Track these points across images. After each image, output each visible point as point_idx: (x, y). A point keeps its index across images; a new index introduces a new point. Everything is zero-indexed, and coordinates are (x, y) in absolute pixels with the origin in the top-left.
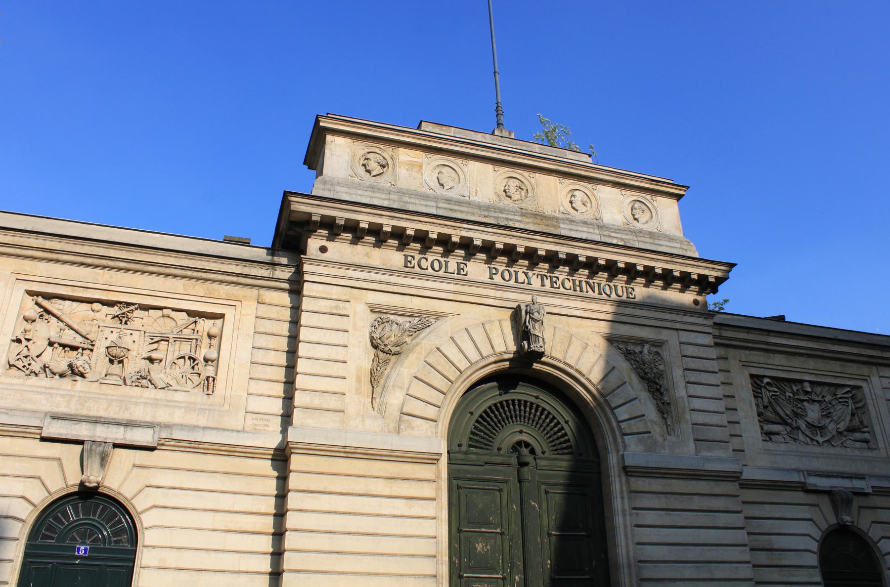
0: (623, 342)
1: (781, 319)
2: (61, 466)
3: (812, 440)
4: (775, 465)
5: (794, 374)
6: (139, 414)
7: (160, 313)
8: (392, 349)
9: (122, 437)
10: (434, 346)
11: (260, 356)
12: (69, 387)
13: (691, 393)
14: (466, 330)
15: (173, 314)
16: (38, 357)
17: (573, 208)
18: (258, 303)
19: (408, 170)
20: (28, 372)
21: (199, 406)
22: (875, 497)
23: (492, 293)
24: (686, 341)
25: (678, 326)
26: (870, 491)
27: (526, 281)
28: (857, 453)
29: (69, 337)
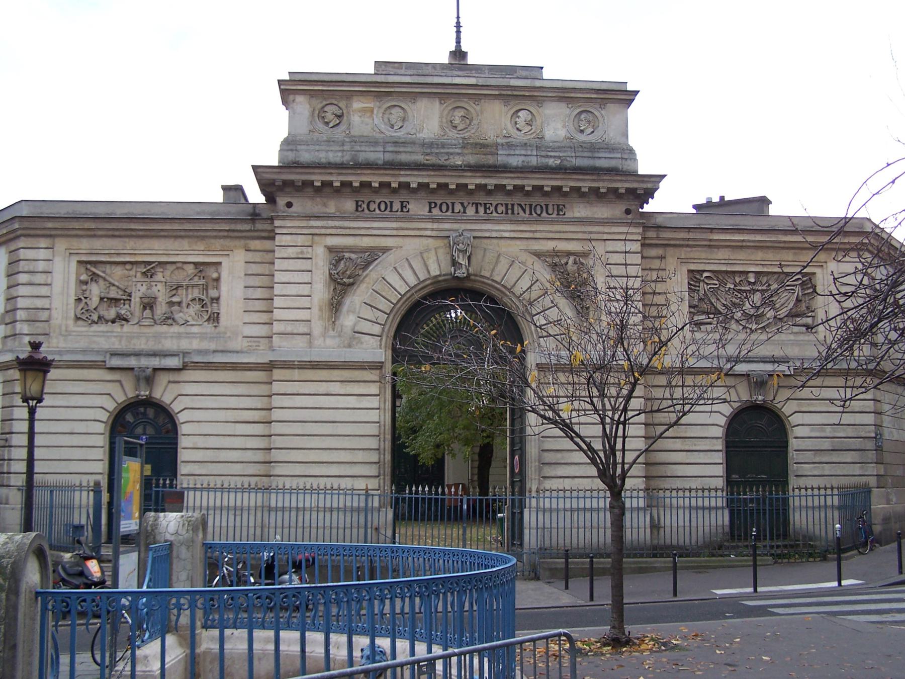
2: (122, 386)
5: (738, 266)
6: (169, 345)
7: (174, 267)
11: (252, 293)
12: (119, 330)
14: (407, 259)
15: (185, 266)
16: (95, 309)
17: (518, 129)
19: (360, 117)
20: (90, 322)
21: (209, 336)
23: (429, 225)
25: (605, 237)
27: (462, 210)
29: (113, 294)
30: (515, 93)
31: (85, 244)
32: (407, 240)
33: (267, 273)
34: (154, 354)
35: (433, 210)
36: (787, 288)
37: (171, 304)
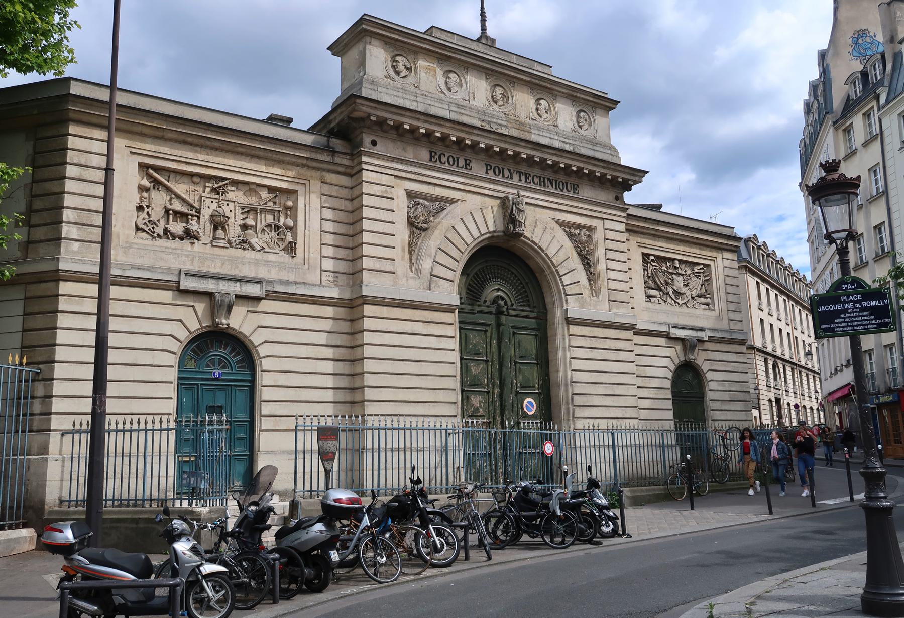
0: (568, 226)
1: (657, 208)
3: (675, 302)
4: (652, 320)
5: (671, 254)
8: (422, 225)
9: (239, 290)
10: (450, 225)
13: (609, 267)
14: (471, 213)
18: (322, 182)
19: (426, 74)
21: (287, 265)
22: (709, 343)
24: (608, 228)
25: (604, 216)
26: (707, 339)
28: (701, 312)
29: (177, 206)
30: (542, 83)
31: (150, 147)
32: (469, 195)
33: (343, 209)
34: (235, 280)
35: (489, 171)
36: (696, 274)
37: (245, 227)
